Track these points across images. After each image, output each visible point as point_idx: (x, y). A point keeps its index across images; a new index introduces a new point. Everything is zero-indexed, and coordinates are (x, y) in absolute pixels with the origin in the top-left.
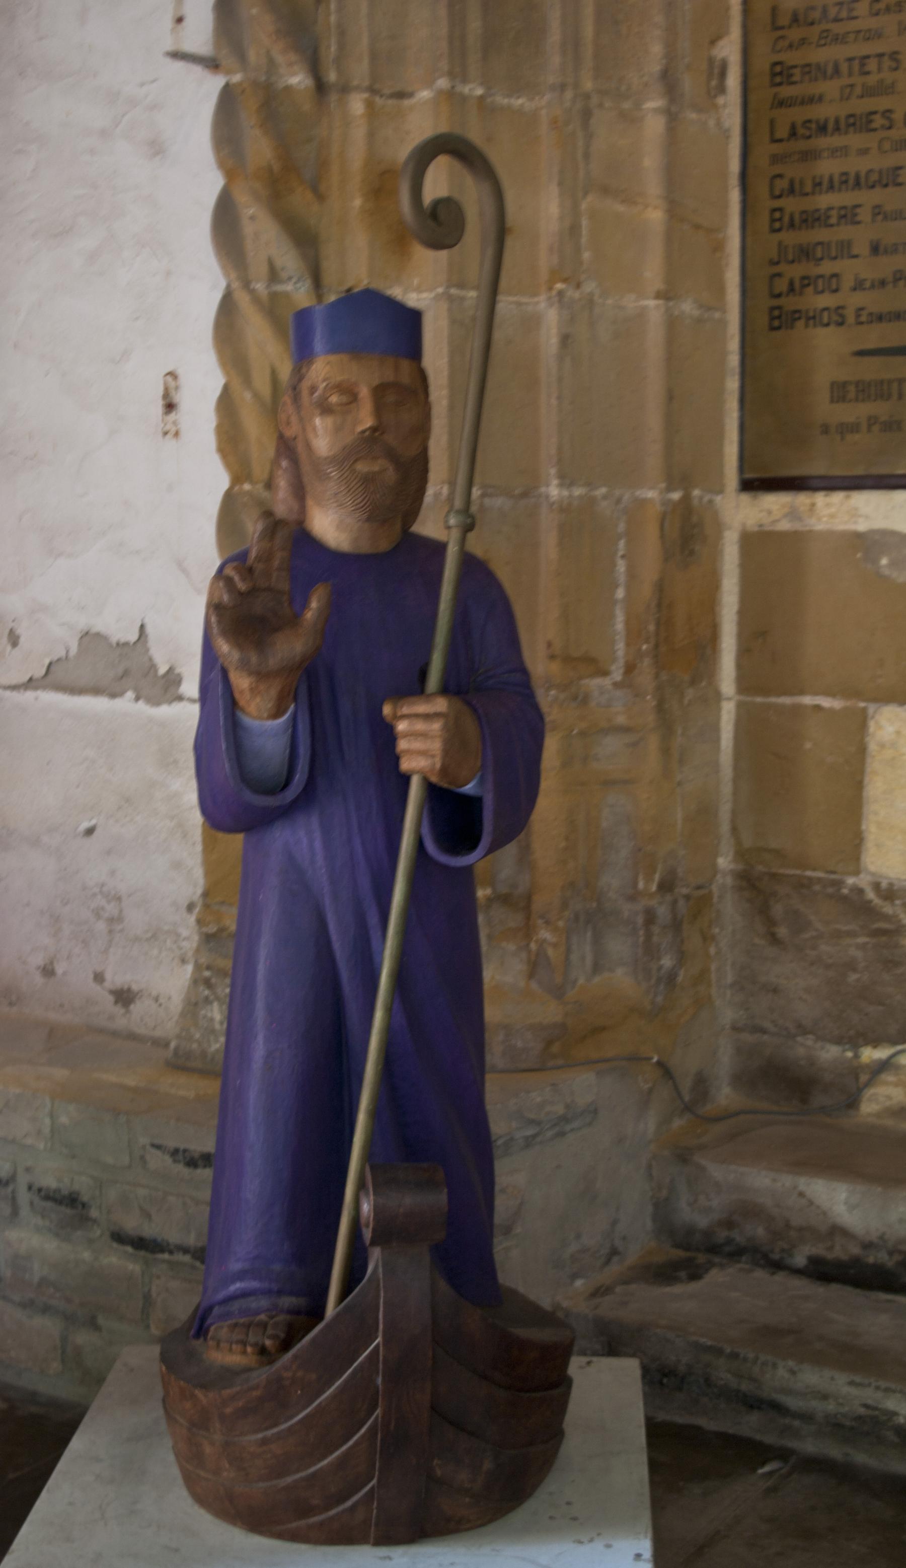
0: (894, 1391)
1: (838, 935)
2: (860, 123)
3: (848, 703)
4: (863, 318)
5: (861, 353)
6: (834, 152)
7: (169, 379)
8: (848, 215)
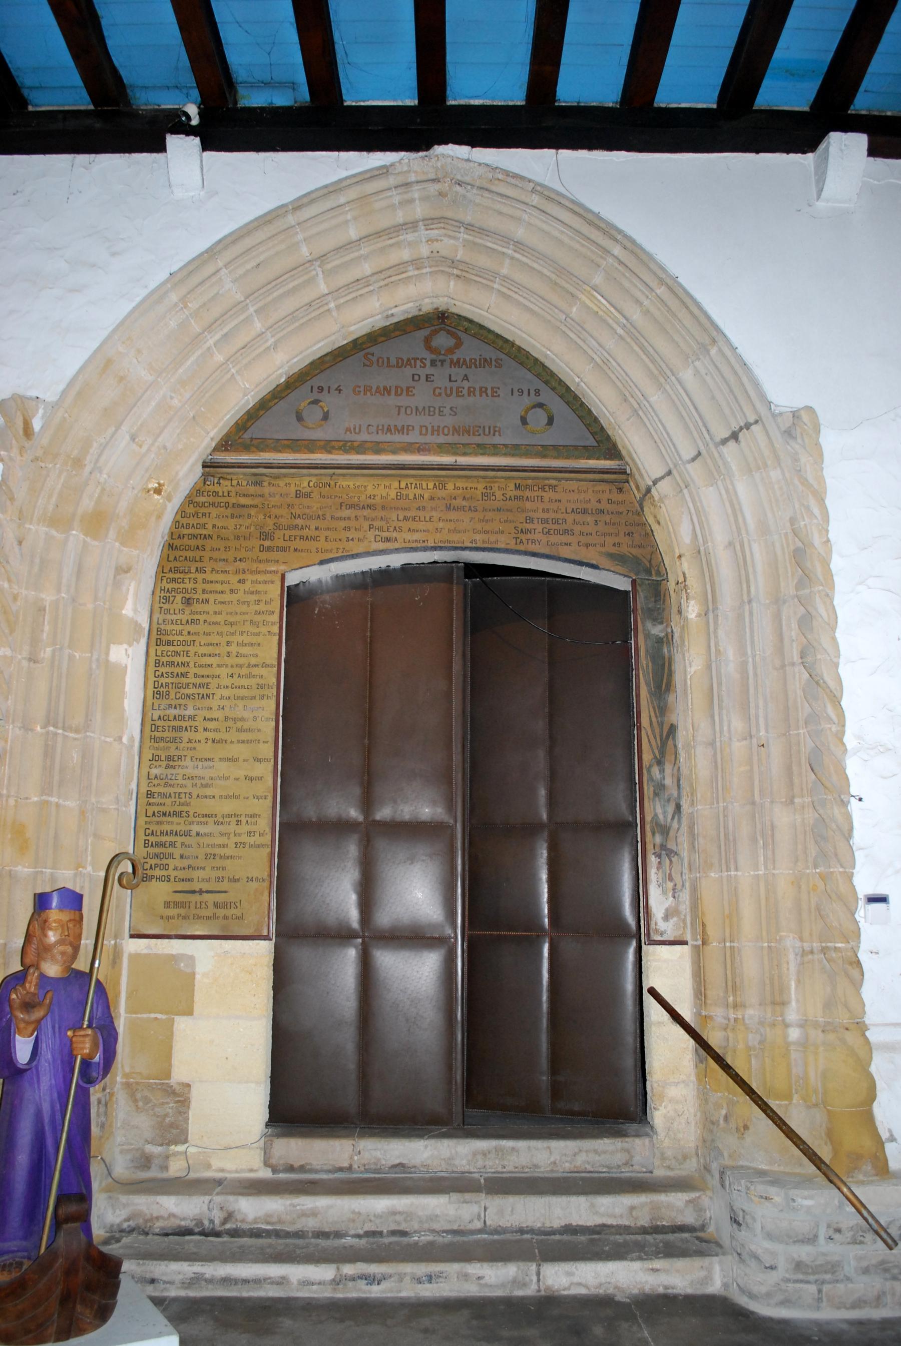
1: (163, 1104)
2: (179, 814)
6: (168, 823)
8: (173, 844)
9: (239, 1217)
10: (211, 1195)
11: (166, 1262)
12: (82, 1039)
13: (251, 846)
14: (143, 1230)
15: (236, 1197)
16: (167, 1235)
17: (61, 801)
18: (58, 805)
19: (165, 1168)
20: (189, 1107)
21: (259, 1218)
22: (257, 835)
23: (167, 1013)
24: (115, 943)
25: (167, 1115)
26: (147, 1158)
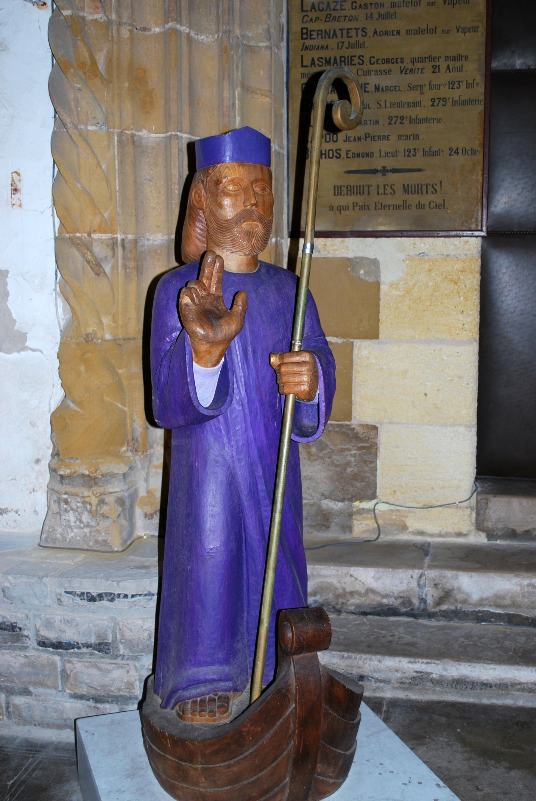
0: (430, 663)
3: (345, 340)
4: (350, 155)
5: (349, 172)
7: (14, 174)
9: (459, 597)
10: (421, 568)
11: (378, 657)
12: (296, 369)
13: (454, 103)
14: (334, 607)
15: (454, 572)
16: (365, 614)
17: (192, 34)
18: (189, 39)
19: (349, 528)
20: (376, 455)
21: (487, 599)
22: (463, 86)
23: (343, 337)
24: (276, 241)
25: (348, 464)
26: (325, 515)
